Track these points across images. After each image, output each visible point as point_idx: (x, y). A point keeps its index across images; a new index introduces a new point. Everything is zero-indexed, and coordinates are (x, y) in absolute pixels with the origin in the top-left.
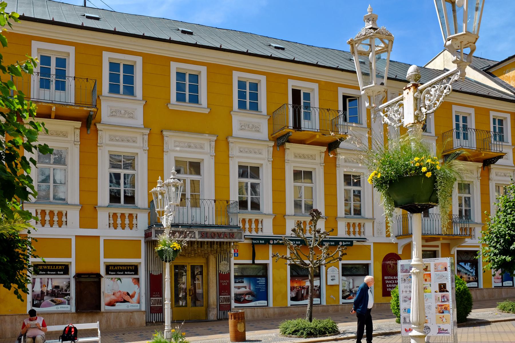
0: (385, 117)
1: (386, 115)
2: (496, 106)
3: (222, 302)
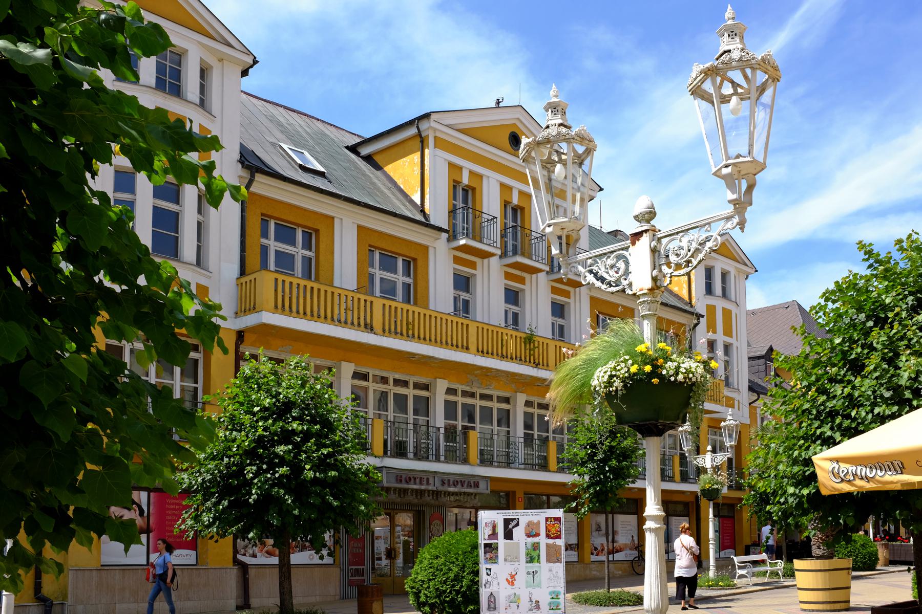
0: (587, 274)
1: (591, 272)
2: (386, 191)
3: (352, 576)
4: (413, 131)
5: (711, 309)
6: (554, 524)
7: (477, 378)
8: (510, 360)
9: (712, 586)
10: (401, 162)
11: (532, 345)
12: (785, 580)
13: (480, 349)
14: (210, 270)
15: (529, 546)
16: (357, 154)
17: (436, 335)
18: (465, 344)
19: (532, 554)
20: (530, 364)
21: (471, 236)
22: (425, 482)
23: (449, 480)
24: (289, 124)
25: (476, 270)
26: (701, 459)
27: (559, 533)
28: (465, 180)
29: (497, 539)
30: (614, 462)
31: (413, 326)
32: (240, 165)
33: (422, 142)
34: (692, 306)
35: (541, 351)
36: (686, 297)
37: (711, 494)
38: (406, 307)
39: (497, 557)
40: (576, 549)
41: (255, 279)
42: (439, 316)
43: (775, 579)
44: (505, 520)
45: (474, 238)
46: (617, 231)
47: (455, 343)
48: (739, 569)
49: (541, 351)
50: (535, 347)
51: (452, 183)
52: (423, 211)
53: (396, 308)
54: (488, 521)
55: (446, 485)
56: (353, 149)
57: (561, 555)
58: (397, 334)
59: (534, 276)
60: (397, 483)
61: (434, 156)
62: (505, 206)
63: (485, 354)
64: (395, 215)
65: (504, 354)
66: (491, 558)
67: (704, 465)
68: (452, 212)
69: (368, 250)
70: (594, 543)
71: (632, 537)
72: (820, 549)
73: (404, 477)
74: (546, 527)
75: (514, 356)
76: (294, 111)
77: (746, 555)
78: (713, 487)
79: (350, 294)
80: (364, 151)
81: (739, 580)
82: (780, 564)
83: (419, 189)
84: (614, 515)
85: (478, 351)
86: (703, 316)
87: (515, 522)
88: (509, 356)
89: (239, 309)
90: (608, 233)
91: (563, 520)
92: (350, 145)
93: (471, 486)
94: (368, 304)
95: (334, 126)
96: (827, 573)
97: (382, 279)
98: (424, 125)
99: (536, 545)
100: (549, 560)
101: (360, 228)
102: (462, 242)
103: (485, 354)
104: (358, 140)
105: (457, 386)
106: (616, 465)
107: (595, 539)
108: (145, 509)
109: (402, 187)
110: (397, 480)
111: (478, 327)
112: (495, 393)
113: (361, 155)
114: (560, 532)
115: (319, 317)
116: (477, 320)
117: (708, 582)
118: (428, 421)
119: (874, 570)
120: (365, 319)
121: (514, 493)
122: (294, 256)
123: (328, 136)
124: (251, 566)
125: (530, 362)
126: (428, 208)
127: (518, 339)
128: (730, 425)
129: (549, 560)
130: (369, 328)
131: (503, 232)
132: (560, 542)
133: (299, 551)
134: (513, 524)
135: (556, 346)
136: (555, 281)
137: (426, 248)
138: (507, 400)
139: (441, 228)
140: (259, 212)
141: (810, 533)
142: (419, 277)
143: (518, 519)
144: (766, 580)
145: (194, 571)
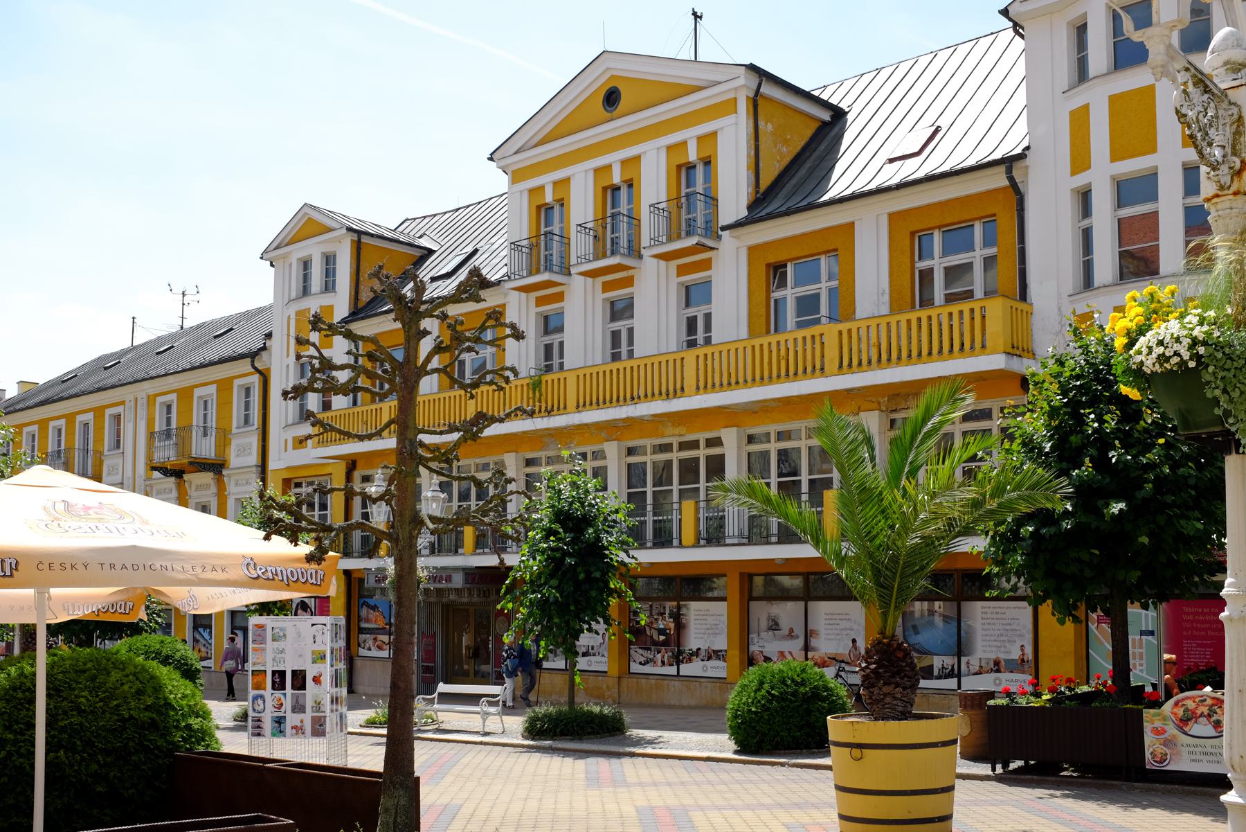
71: (854, 641)
79: (741, 346)
84: (810, 604)
107: (765, 644)
108: (313, 610)
120: (450, 419)
138: (711, 443)
139: (43, 405)
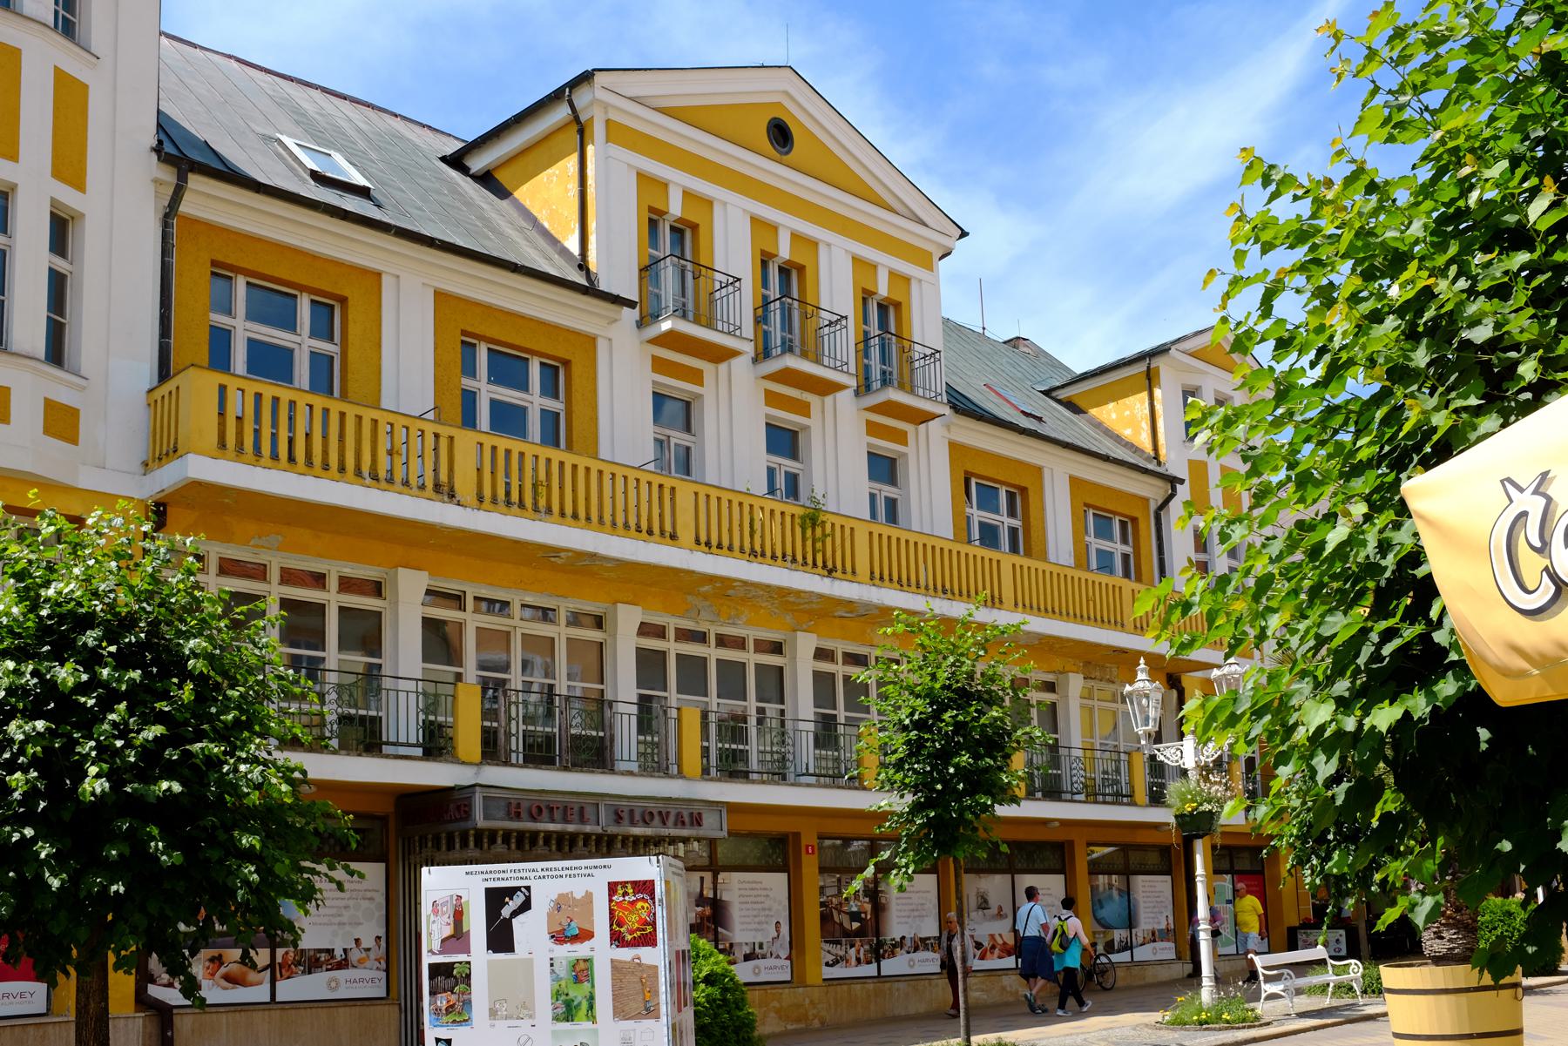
4: (561, 113)
5: (1198, 469)
6: (633, 903)
7: (708, 603)
8: (771, 562)
9: (1207, 1023)
10: (543, 176)
11: (819, 531)
12: (1366, 1000)
13: (703, 539)
14: (83, 373)
15: (563, 971)
16: (464, 170)
17: (575, 502)
18: (668, 528)
19: (572, 995)
20: (815, 570)
21: (691, 316)
22: (576, 817)
23: (632, 812)
24: (322, 115)
25: (702, 386)
26: (1173, 750)
27: (649, 929)
28: (675, 208)
29: (467, 951)
30: (965, 759)
31: (549, 487)
32: (154, 157)
33: (581, 132)
34: (1159, 464)
35: (838, 541)
36: (1145, 441)
37: (1197, 824)
38: (547, 452)
39: (467, 1003)
40: (936, 948)
41: (178, 388)
42: (619, 472)
43: (1347, 1000)
44: (489, 892)
45: (697, 321)
46: (1018, 338)
47: (644, 526)
48: (1266, 982)
49: (838, 541)
50: (825, 535)
51: (646, 215)
52: (583, 266)
53: (508, 452)
54: (441, 896)
55: (626, 821)
56: (456, 161)
57: (657, 993)
58: (510, 503)
59: (829, 399)
60: (511, 819)
61: (604, 160)
62: (764, 264)
63: (714, 549)
64: (514, 268)
65: (758, 548)
66: (450, 1009)
67: (1181, 762)
68: (648, 270)
69: (459, 345)
70: (975, 934)
72: (1442, 938)
73: (525, 805)
74: (611, 912)
75: (779, 554)
76: (344, 97)
77: (1290, 950)
78: (1201, 808)
80: (477, 163)
81: (1271, 1004)
82: (1355, 968)
83: (577, 225)
85: (698, 542)
86: (1182, 481)
87: (519, 899)
88: (769, 554)
89: (151, 455)
90: (1005, 343)
91: (659, 889)
92: (448, 154)
93: (683, 823)
94: (443, 443)
95: (429, 127)
96: (1463, 997)
97: (494, 403)
98: (582, 97)
99: (582, 965)
100: (620, 1012)
101: (440, 296)
102: (666, 326)
103: (714, 549)
104: (460, 145)
105: (666, 620)
106: (969, 764)
107: (976, 926)
109: (546, 225)
110: (508, 813)
111: (696, 494)
112: (751, 634)
113: (472, 172)
114: (654, 924)
115: (326, 467)
116: (708, 481)
117: (1199, 1015)
118: (602, 690)
119: (1555, 972)
121: (797, 835)
122: (291, 351)
123: (408, 139)
124: (181, 1011)
125: (815, 565)
126: (595, 260)
127: (788, 519)
128: (1231, 674)
129: (620, 1012)
130: (446, 491)
131: (760, 312)
132: (655, 957)
133: (303, 972)
134: (513, 904)
135: (871, 533)
136: (873, 409)
137: (592, 340)
140: (205, 259)
141: (1413, 906)
142: (577, 397)
143: (528, 888)
144: (1327, 1002)
145: (31, 1030)
